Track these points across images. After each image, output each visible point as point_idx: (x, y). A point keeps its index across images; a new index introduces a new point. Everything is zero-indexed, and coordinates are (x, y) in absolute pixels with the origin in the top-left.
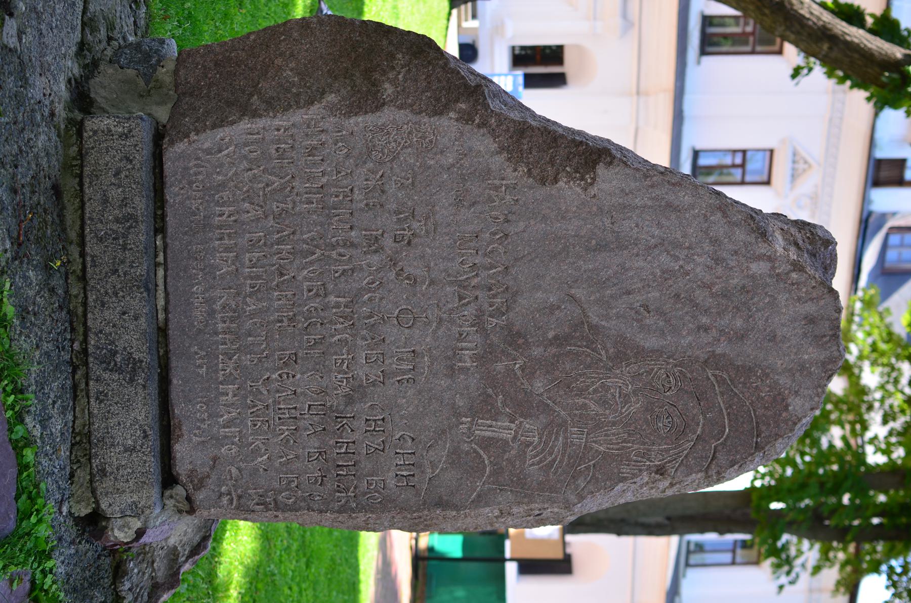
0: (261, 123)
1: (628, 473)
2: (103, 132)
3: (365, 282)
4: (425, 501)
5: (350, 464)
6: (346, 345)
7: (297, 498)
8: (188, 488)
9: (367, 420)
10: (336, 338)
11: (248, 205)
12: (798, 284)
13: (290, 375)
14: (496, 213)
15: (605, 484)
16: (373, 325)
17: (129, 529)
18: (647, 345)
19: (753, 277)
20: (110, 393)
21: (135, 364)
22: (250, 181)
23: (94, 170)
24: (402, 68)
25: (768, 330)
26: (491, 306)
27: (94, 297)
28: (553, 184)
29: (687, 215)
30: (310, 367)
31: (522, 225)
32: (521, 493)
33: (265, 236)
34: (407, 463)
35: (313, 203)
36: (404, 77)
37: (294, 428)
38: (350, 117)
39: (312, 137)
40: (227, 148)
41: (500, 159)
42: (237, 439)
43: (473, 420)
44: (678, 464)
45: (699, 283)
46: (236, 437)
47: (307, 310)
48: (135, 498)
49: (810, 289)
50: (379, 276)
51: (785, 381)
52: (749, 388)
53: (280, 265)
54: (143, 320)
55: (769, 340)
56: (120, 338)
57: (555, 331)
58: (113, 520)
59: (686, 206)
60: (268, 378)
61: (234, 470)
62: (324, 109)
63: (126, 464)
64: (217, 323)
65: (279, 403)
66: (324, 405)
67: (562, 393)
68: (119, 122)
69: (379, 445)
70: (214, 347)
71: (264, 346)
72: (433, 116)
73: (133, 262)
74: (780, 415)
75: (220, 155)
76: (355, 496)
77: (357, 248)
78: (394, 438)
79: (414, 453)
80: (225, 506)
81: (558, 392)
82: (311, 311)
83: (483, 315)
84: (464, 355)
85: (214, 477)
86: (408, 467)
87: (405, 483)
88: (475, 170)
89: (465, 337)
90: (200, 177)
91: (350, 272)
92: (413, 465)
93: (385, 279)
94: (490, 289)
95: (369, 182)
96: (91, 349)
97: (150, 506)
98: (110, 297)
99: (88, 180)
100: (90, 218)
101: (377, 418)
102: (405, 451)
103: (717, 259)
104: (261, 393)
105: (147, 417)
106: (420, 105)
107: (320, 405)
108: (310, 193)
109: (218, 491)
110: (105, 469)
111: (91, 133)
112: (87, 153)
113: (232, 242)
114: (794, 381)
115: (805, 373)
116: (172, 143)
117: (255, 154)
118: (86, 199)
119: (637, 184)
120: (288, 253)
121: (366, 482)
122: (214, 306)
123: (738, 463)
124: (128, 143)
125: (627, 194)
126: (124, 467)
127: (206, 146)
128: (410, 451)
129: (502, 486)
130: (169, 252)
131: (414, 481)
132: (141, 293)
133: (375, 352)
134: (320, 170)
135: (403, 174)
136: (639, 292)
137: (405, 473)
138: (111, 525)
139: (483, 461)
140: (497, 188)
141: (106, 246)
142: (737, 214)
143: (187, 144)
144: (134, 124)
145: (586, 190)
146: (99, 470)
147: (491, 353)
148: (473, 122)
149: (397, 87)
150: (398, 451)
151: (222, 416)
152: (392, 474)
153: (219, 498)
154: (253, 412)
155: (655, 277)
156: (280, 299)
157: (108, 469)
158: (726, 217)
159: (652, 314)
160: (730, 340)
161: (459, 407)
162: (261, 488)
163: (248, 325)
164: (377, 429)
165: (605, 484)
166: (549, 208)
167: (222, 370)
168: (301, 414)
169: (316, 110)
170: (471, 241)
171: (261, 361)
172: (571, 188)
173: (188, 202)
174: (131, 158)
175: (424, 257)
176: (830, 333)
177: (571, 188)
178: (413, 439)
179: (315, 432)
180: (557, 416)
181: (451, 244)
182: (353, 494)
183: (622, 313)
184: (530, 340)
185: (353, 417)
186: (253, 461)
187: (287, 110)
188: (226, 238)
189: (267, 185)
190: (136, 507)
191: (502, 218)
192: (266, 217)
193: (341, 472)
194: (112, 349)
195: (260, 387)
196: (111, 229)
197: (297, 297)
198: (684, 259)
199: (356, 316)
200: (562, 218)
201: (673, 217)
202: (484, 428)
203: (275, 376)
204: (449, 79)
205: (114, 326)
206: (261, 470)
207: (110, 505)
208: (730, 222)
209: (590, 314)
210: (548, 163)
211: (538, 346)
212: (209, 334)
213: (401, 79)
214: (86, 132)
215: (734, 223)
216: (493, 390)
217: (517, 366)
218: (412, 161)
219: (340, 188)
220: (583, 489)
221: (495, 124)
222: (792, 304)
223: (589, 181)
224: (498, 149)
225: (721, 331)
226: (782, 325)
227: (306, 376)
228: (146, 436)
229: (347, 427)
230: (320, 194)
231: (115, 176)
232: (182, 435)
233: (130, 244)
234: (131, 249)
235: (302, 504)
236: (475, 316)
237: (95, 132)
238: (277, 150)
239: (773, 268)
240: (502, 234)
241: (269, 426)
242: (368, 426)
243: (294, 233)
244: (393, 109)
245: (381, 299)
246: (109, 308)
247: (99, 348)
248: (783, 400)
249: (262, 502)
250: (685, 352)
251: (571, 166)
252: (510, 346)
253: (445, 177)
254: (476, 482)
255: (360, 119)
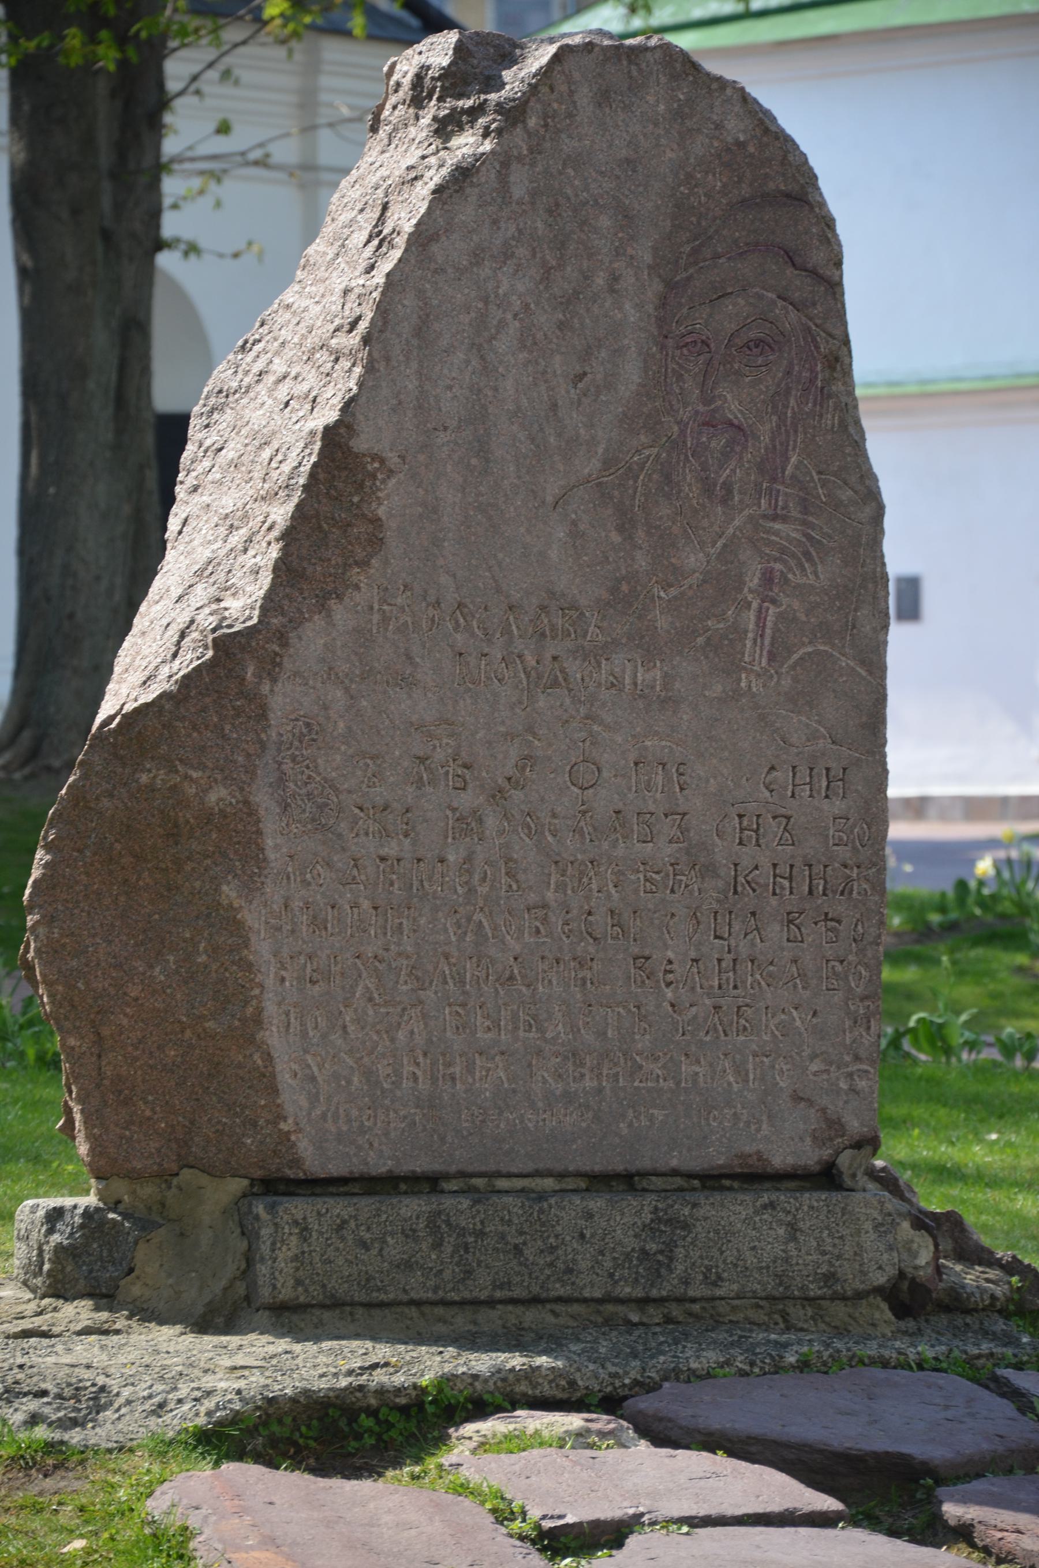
0: (271, 1008)
1: (833, 417)
2: (297, 1269)
3: (527, 840)
4: (868, 752)
5: (807, 873)
6: (623, 874)
7: (859, 963)
8: (842, 1146)
9: (740, 843)
10: (613, 891)
11: (400, 1033)
12: (545, 116)
13: (668, 967)
14: (424, 621)
15: (849, 455)
16: (595, 829)
17: (912, 1241)
18: (636, 379)
19: (534, 194)
20: (706, 1262)
21: (660, 1220)
22: (363, 1028)
23: (359, 1284)
24: (177, 772)
25: (617, 172)
26: (569, 635)
27: (557, 1285)
28: (381, 526)
29: (435, 302)
30: (657, 934)
31: (444, 579)
32: (860, 595)
33: (450, 1005)
34: (808, 780)
35: (401, 924)
36: (195, 769)
37: (750, 964)
38: (265, 860)
39: (295, 923)
40: (309, 1066)
41: (339, 612)
42: (765, 1059)
43: (745, 669)
44: (822, 333)
45: (541, 287)
46: (762, 1062)
47: (568, 937)
48: (868, 1226)
49: (553, 97)
50: (518, 817)
51: (699, 146)
52: (708, 209)
53: (497, 980)
54: (592, 1204)
55: (634, 171)
56: (620, 1243)
57: (610, 531)
58: (902, 1265)
59: (420, 303)
60: (673, 1005)
61: (814, 1067)
62: (251, 902)
63: (815, 1238)
64: (585, 1088)
65: (712, 987)
66: (716, 913)
67: (705, 523)
68: (283, 1241)
69: (780, 823)
70: (622, 1095)
71: (621, 1010)
72: (267, 719)
73: (502, 1219)
74: (752, 156)
75: (319, 1079)
76: (858, 867)
77: (473, 852)
78: (770, 800)
79: (794, 768)
80: (870, 1083)
81: (704, 529)
82: (570, 931)
83: (583, 648)
84: (644, 680)
85: (825, 1101)
86: (815, 779)
87: (840, 783)
88: (356, 654)
89: (615, 678)
90: (355, 1113)
91: (511, 864)
92: (811, 769)
93: (523, 807)
94: (543, 635)
95: (371, 830)
96: (639, 1293)
97: (880, 1202)
98: (558, 1258)
99: (375, 1294)
100: (435, 1292)
101: (737, 826)
102: (790, 781)
103: (505, 254)
104: (695, 1017)
105: (742, 1201)
106: (248, 742)
107: (715, 920)
108: (385, 928)
109: (847, 1094)
110: (823, 1274)
111: (300, 1289)
112: (333, 1296)
113: (458, 1060)
114: (699, 131)
115: (687, 110)
116: (296, 1162)
117: (319, 1019)
118: (405, 1298)
119: (384, 384)
120: (478, 966)
121: (835, 848)
122: (558, 1093)
123: (824, 232)
124: (316, 1227)
125: (400, 403)
126: (820, 1241)
127: (304, 1102)
128: (791, 774)
129: (847, 626)
130: (470, 1169)
131: (837, 772)
132: (550, 1207)
133: (635, 827)
134: (349, 911)
135: (359, 773)
136: (553, 390)
137: (824, 784)
138: (910, 1270)
139: (809, 654)
140: (385, 619)
141: (479, 1265)
142: (434, 216)
143: (300, 1135)
144: (286, 1217)
145: (391, 471)
146: (826, 1286)
147: (642, 637)
148: (276, 654)
149: (216, 781)
150: (789, 794)
151: (729, 1084)
152: (825, 805)
153: (858, 1093)
154: (724, 1031)
155: (530, 361)
156: (550, 981)
157: (824, 1269)
158: (438, 235)
159: (588, 369)
160: (632, 238)
161: (724, 691)
162: (844, 1022)
163: (588, 1037)
164: (755, 826)
165: (849, 455)
166: (418, 533)
167: (658, 1081)
168: (729, 952)
169: (252, 917)
170: (468, 663)
171: (645, 1016)
172: (388, 496)
173: (393, 1135)
174: (338, 1221)
175: (490, 743)
176: (625, 63)
177: (388, 496)
178: (772, 768)
179: (757, 929)
180: (741, 531)
181: (471, 697)
182: (855, 870)
183: (584, 419)
184: (624, 572)
185: (736, 865)
186: (800, 1034)
187: (250, 965)
188: (452, 1070)
189: (371, 999)
190: (882, 1225)
191: (431, 612)
192: (421, 1002)
193: (821, 888)
194: (638, 1258)
195: (686, 1020)
196: (452, 1257)
197: (546, 954)
198: (504, 312)
199: (579, 857)
200: (435, 513)
201: (436, 326)
202: (758, 651)
203: (669, 994)
204: (200, 693)
205: (602, 1253)
206: (814, 1021)
207: (880, 1268)
208: (447, 231)
209: (586, 471)
210: (346, 531)
211: (633, 560)
212: (600, 1102)
213: (200, 774)
214: (298, 1298)
215: (448, 223)
216: (700, 635)
217: (662, 594)
218: (338, 757)
219: (378, 877)
220: (856, 492)
221: (280, 618)
222: (577, 127)
223: (376, 465)
224: (323, 614)
225: (618, 254)
226: (610, 146)
227: (670, 942)
228: (772, 1205)
229: (751, 876)
230: (386, 911)
231: (368, 1249)
232: (758, 1152)
233: (474, 1224)
234: (482, 1222)
235: (869, 953)
236: (584, 660)
237: (298, 1282)
238: (313, 982)
239: (520, 159)
240: (458, 612)
241: (747, 1005)
242: (750, 842)
243: (447, 956)
244: (255, 787)
245: (554, 816)
246: (574, 1261)
247: (636, 1279)
248: (728, 150)
249: (865, 1020)
250: (649, 316)
251: (351, 495)
252: (631, 605)
253: (365, 703)
254: (841, 667)
255: (270, 842)
